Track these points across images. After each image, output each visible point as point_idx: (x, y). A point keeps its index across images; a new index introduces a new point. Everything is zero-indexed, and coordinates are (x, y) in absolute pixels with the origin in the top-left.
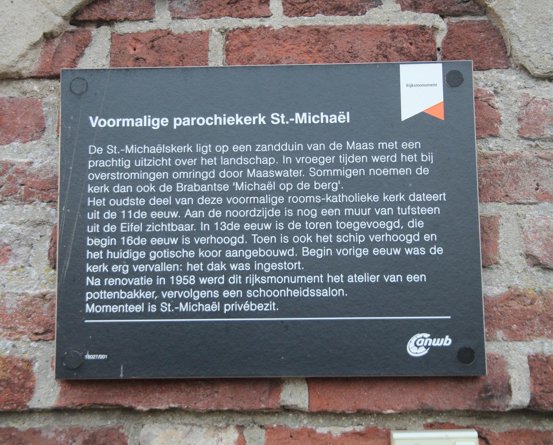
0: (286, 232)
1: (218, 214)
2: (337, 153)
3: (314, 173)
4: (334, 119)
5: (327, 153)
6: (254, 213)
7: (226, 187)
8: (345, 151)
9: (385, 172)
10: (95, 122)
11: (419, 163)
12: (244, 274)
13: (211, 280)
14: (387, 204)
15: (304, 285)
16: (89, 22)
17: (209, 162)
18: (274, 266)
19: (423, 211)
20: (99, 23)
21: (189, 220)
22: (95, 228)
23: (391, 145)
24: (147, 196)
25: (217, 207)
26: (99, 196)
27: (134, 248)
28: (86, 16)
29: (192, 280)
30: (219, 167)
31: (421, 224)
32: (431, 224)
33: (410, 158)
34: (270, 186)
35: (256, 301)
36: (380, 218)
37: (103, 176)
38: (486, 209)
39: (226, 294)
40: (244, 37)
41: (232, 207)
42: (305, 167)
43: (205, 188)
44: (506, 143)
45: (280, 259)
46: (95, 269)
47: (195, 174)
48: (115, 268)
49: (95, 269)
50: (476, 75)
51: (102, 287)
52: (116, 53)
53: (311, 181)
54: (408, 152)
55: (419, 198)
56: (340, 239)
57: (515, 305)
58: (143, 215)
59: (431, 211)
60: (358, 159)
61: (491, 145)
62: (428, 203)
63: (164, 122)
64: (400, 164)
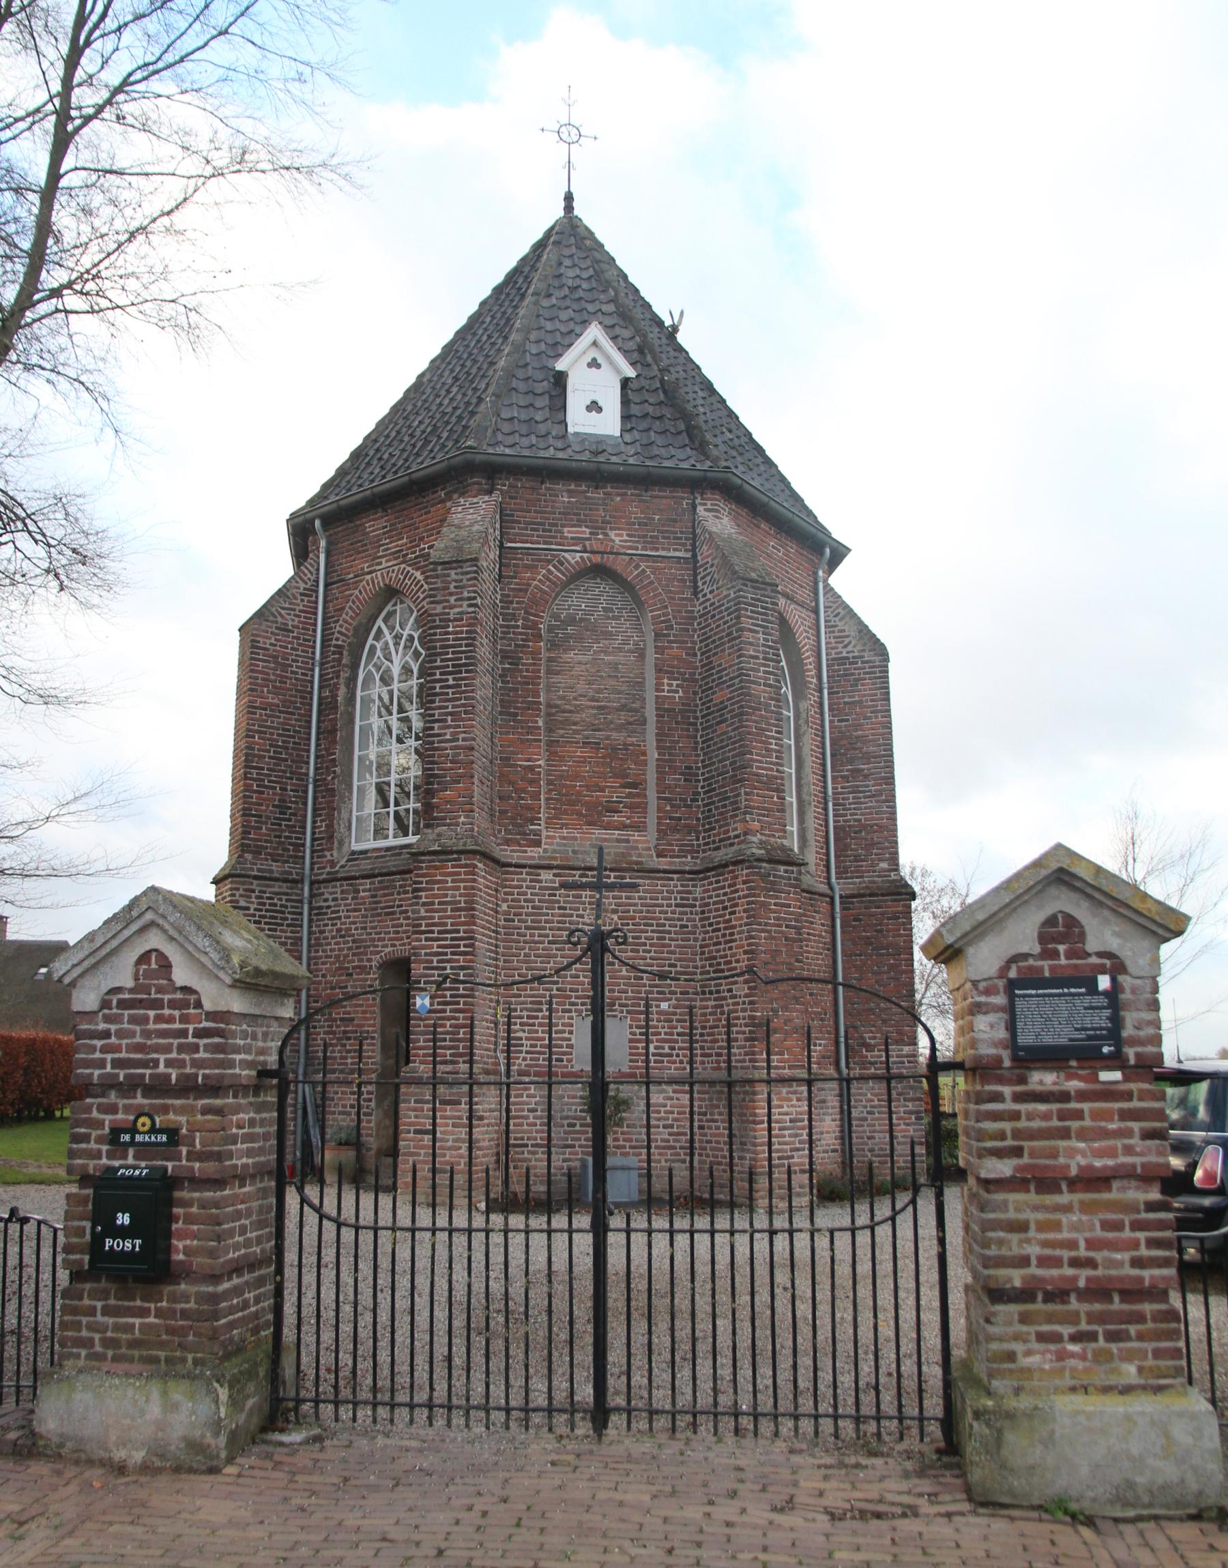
62: (1107, 1013)
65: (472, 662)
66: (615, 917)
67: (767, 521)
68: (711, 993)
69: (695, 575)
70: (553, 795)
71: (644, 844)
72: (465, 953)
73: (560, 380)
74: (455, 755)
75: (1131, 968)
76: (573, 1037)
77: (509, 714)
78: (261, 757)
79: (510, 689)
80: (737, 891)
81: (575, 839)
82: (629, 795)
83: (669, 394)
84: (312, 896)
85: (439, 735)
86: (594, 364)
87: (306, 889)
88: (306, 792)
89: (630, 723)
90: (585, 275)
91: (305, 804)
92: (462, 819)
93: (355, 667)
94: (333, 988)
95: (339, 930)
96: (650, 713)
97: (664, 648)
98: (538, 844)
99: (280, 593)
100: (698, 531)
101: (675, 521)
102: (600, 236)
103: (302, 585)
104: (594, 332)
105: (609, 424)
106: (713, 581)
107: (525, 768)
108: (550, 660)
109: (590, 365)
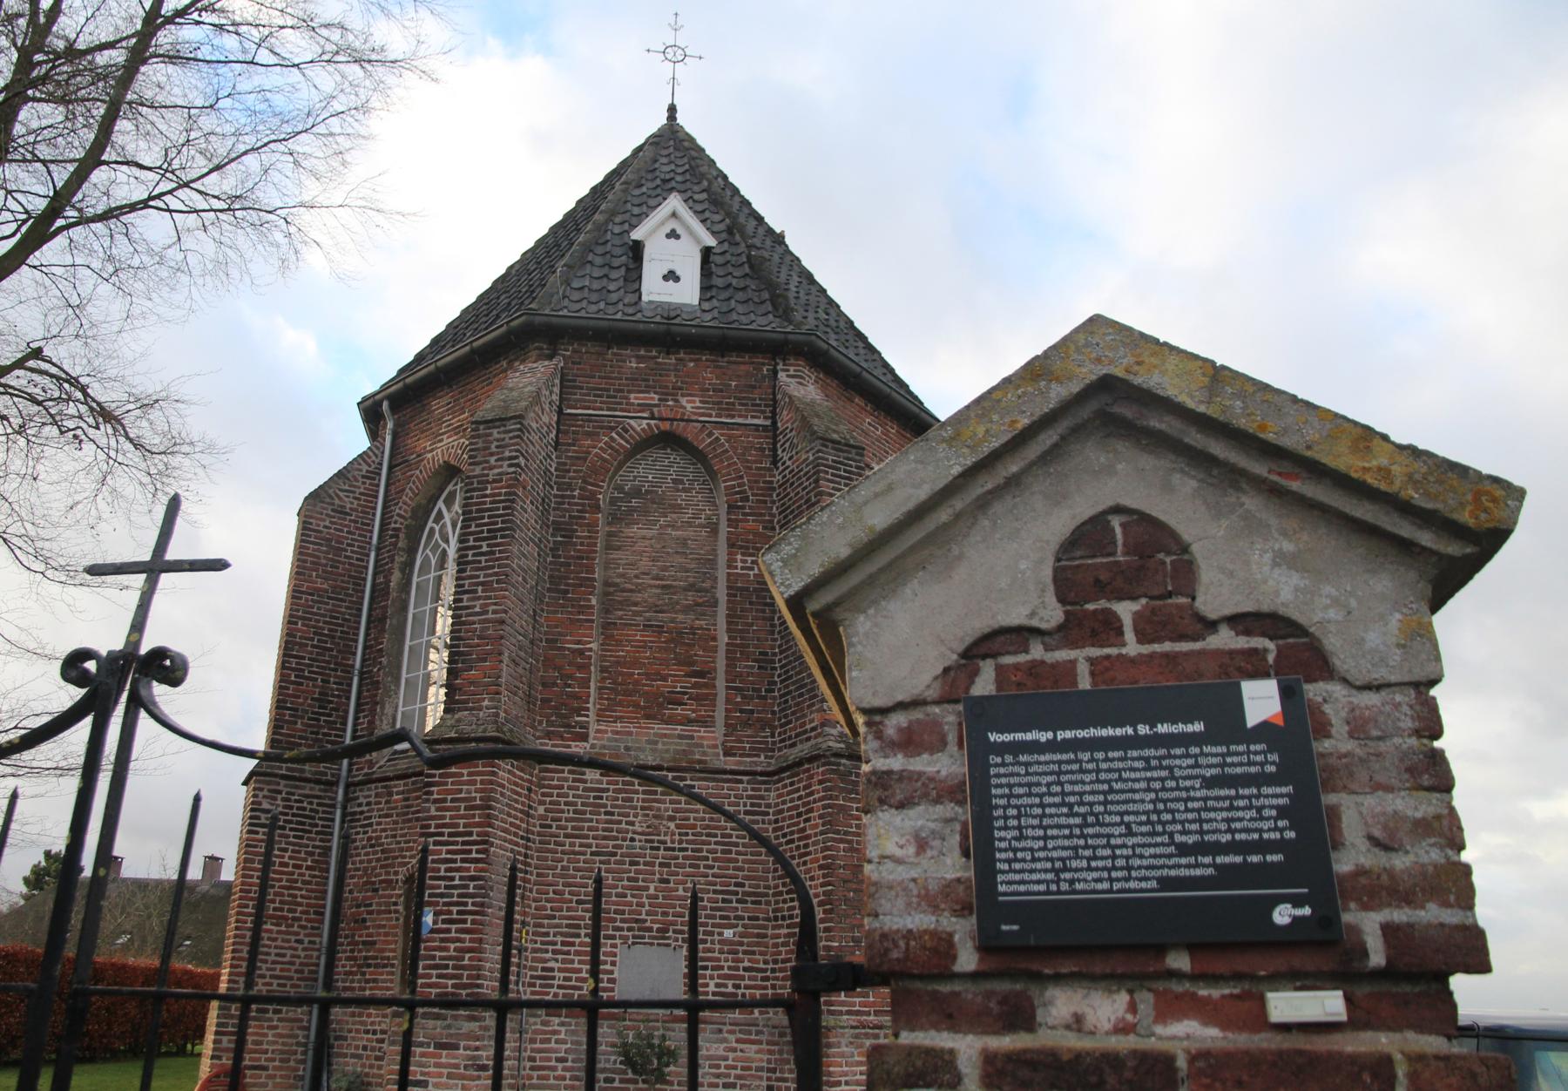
0: (1159, 822)
1: (1101, 809)
2: (1196, 756)
3: (1178, 773)
4: (1190, 728)
5: (1187, 756)
6: (1131, 807)
7: (1106, 787)
8: (1202, 754)
9: (1239, 770)
10: (993, 737)
11: (1267, 762)
12: (1127, 858)
13: (1100, 864)
14: (1243, 797)
15: (1180, 866)
16: (977, 656)
17: (1090, 766)
18: (1152, 851)
19: (1275, 802)
20: (984, 657)
21: (1077, 815)
22: (1000, 823)
23: (1241, 748)
24: (1041, 796)
25: (1099, 803)
26: (1002, 796)
27: (1034, 838)
28: (975, 651)
29: (1084, 863)
30: (1098, 771)
31: (1274, 813)
32: (1282, 812)
33: (1259, 758)
34: (1143, 785)
35: (1141, 879)
36: (1238, 809)
37: (1004, 780)
38: (1329, 799)
39: (1114, 874)
40: (1106, 663)
41: (1112, 803)
42: (1170, 769)
43: (1088, 788)
44: (1338, 743)
45: (1156, 845)
46: (1003, 856)
47: (1079, 777)
48: (1020, 855)
49: (1003, 856)
50: (1306, 687)
51: (1011, 871)
52: (1000, 680)
53: (1176, 779)
54: (1256, 753)
55: (1270, 791)
56: (1205, 827)
57: (1363, 880)
58: (1039, 811)
59: (1281, 801)
60: (1214, 760)
61: (1327, 745)
62: (1278, 795)
63: (1050, 735)
64: (1250, 764)
65: (509, 529)
66: (672, 825)
67: (861, 395)
68: (783, 918)
69: (775, 444)
70: (608, 683)
71: (710, 741)
72: (477, 861)
73: (637, 250)
74: (483, 630)
75: (1343, 660)
76: (616, 969)
77: (558, 591)
78: (303, 646)
79: (562, 564)
80: (812, 793)
81: (630, 733)
82: (695, 686)
83: (756, 268)
84: (347, 799)
85: (467, 608)
86: (673, 235)
87: (341, 792)
88: (350, 685)
89: (697, 604)
90: (680, 170)
91: (348, 698)
92: (486, 703)
93: (412, 551)
94: (358, 906)
95: (370, 839)
96: (722, 594)
97: (738, 521)
98: (584, 737)
99: (341, 474)
100: (779, 397)
101: (754, 387)
102: (700, 142)
103: (365, 467)
104: (674, 202)
105: (687, 293)
106: (792, 446)
107: (573, 651)
108: (610, 534)
109: (668, 236)
